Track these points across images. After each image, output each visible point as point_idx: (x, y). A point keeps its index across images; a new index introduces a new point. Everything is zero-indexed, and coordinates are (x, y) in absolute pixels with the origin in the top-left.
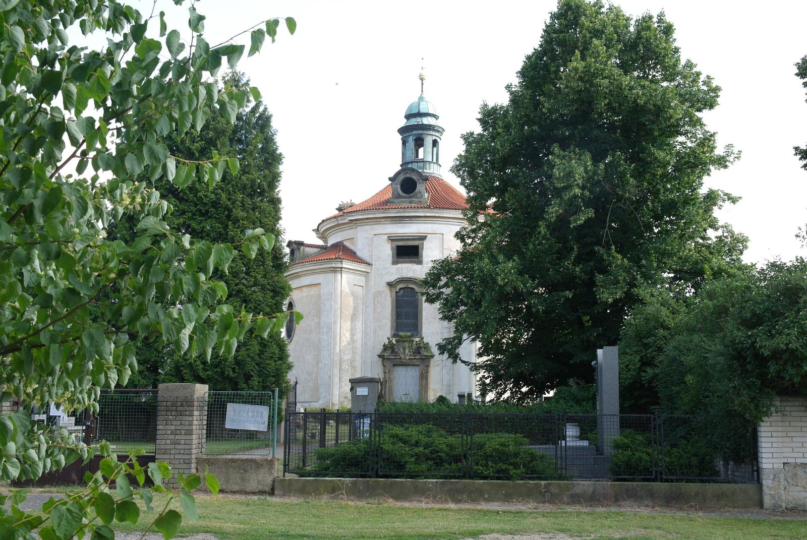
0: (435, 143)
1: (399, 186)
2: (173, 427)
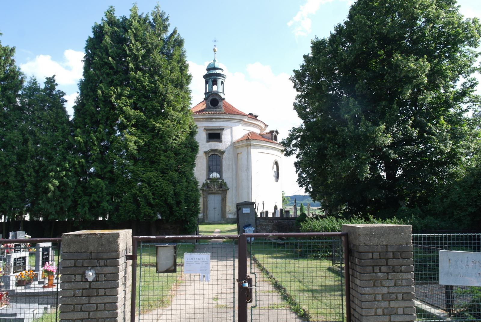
0: (222, 83)
1: (209, 102)
2: (385, 290)
